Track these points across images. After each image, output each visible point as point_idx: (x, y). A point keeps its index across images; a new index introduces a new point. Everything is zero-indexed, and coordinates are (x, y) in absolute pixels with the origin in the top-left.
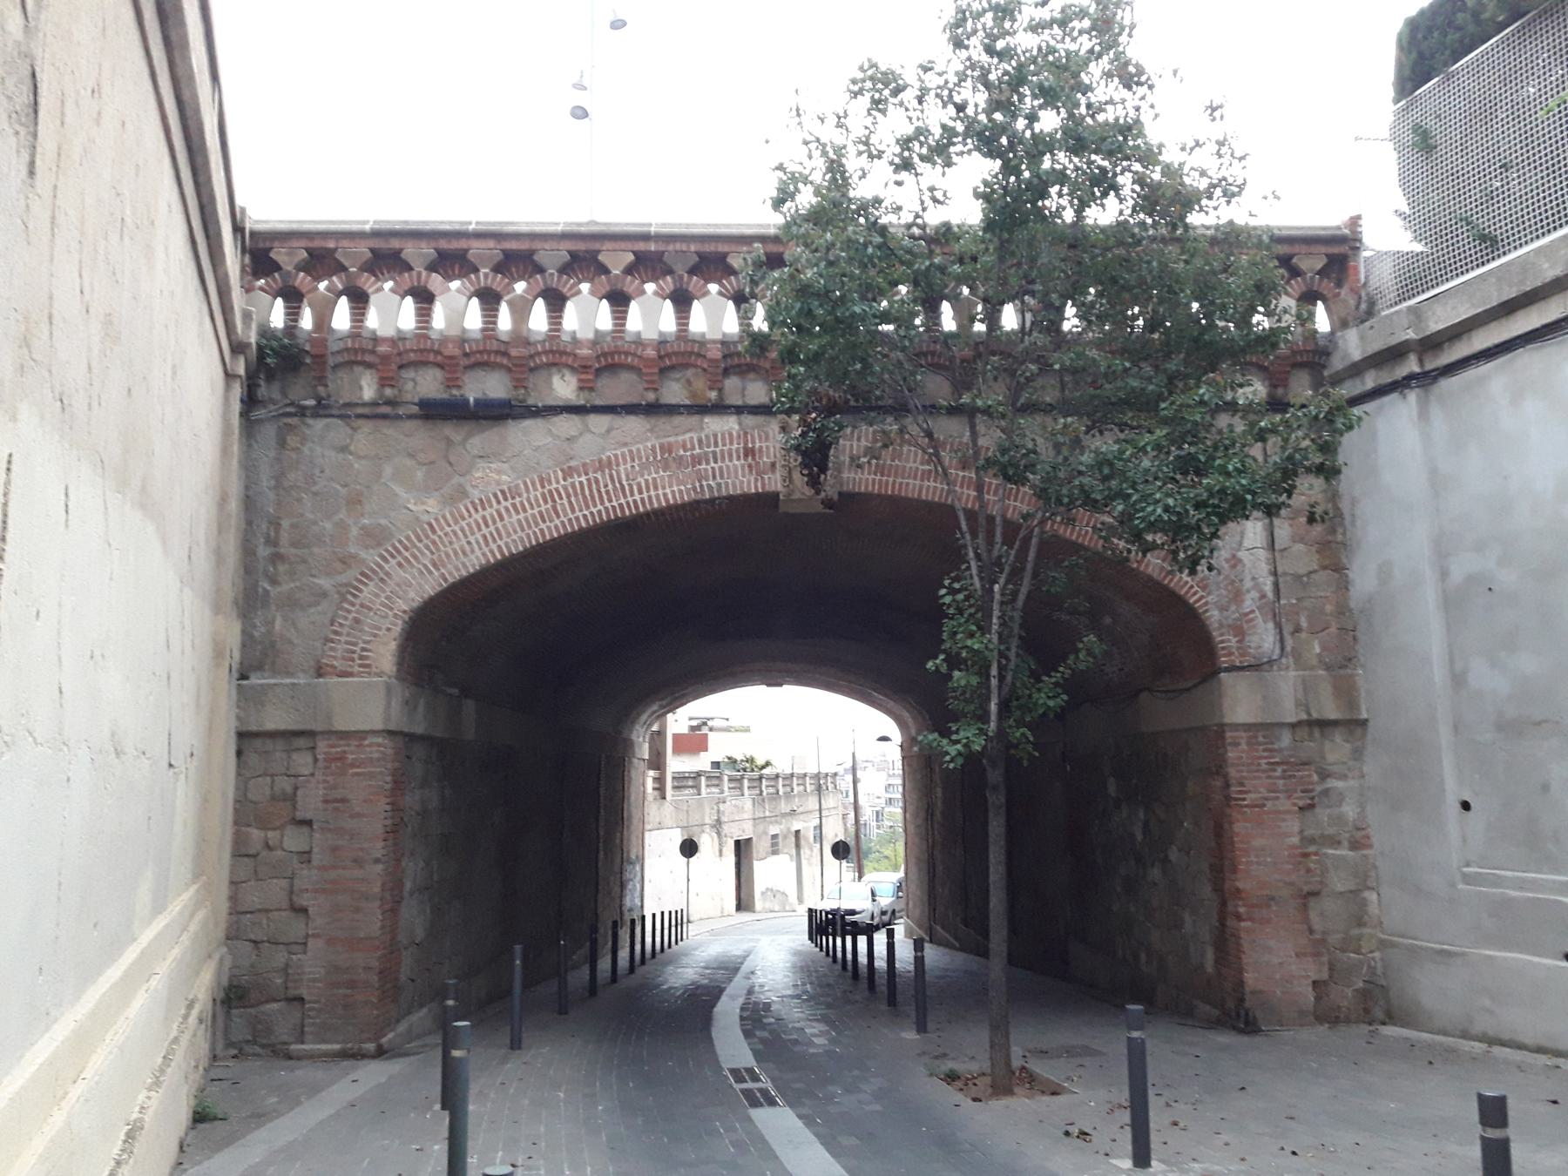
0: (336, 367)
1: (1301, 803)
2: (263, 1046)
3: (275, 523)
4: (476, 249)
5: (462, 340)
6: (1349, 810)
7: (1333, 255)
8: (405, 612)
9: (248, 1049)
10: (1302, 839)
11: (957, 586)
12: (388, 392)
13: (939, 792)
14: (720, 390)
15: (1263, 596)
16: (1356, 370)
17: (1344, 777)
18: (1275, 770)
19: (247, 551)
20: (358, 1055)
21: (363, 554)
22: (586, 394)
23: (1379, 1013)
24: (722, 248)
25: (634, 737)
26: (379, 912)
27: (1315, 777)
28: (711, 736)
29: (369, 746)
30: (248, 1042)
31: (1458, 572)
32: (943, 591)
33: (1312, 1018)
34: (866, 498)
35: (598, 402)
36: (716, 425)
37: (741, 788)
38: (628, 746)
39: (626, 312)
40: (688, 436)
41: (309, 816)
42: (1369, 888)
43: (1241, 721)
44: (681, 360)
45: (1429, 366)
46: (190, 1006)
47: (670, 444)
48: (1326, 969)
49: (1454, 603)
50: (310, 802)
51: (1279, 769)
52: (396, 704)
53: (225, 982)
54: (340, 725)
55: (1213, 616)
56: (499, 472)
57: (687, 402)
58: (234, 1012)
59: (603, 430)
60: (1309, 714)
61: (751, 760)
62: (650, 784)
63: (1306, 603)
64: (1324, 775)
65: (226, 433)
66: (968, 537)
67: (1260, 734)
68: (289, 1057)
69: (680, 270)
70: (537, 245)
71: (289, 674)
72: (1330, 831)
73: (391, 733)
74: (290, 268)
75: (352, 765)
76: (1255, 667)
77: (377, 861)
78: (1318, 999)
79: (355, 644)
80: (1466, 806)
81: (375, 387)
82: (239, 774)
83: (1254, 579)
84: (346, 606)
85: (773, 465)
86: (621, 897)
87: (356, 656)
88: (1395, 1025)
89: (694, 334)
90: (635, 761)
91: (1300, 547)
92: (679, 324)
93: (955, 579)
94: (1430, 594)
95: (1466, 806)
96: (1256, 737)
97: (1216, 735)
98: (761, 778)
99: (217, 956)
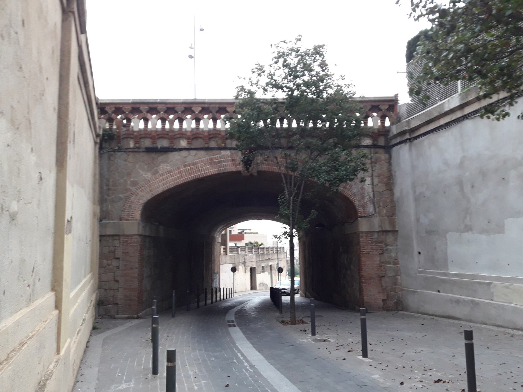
0: (123, 138)
1: (380, 252)
2: (108, 316)
3: (108, 180)
4: (160, 107)
5: (156, 131)
6: (393, 255)
7: (391, 105)
8: (142, 203)
9: (105, 316)
10: (380, 262)
11: (282, 197)
12: (137, 145)
13: (307, 251)
14: (225, 143)
15: (370, 198)
16: (395, 136)
17: (392, 246)
18: (373, 244)
19: (101, 187)
20: (133, 318)
21: (131, 188)
22: (189, 145)
23: (400, 308)
24: (225, 106)
25: (215, 235)
26: (137, 281)
27: (384, 246)
28: (245, 235)
29: (134, 238)
30: (104, 315)
31: (417, 193)
32: (279, 198)
33: (382, 309)
34: (265, 172)
35: (193, 147)
36: (224, 153)
37: (252, 251)
38: (213, 239)
39: (200, 123)
40: (217, 156)
41: (118, 257)
42: (399, 275)
43: (363, 231)
44: (213, 136)
45: (412, 137)
46: (92, 301)
47: (212, 158)
48: (386, 296)
49: (417, 200)
50: (119, 253)
51: (374, 243)
52: (141, 228)
53: (98, 299)
54: (127, 233)
55: (357, 203)
56: (167, 166)
57: (217, 147)
58: (101, 307)
59: (194, 154)
60: (382, 229)
61: (257, 243)
62: (222, 250)
63: (382, 199)
64: (387, 245)
65: (95, 157)
66: (285, 184)
67: (369, 234)
68: (115, 318)
69: (214, 111)
70: (176, 106)
71: (113, 220)
72: (388, 260)
73: (140, 235)
74: (110, 112)
75: (130, 243)
76: (368, 216)
77: (137, 268)
78: (384, 304)
79: (130, 212)
80: (420, 253)
81: (133, 144)
82: (100, 246)
83: (368, 193)
84: (127, 202)
85: (240, 163)
86: (212, 284)
87: (130, 215)
88: (404, 311)
89: (218, 128)
90: (216, 243)
91: (380, 184)
92: (214, 126)
93: (282, 196)
94: (411, 198)
95: (420, 253)
96: (368, 235)
97: (357, 234)
98: (258, 248)
99: (96, 293)
